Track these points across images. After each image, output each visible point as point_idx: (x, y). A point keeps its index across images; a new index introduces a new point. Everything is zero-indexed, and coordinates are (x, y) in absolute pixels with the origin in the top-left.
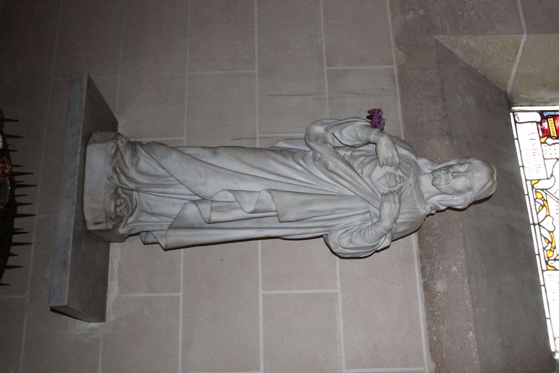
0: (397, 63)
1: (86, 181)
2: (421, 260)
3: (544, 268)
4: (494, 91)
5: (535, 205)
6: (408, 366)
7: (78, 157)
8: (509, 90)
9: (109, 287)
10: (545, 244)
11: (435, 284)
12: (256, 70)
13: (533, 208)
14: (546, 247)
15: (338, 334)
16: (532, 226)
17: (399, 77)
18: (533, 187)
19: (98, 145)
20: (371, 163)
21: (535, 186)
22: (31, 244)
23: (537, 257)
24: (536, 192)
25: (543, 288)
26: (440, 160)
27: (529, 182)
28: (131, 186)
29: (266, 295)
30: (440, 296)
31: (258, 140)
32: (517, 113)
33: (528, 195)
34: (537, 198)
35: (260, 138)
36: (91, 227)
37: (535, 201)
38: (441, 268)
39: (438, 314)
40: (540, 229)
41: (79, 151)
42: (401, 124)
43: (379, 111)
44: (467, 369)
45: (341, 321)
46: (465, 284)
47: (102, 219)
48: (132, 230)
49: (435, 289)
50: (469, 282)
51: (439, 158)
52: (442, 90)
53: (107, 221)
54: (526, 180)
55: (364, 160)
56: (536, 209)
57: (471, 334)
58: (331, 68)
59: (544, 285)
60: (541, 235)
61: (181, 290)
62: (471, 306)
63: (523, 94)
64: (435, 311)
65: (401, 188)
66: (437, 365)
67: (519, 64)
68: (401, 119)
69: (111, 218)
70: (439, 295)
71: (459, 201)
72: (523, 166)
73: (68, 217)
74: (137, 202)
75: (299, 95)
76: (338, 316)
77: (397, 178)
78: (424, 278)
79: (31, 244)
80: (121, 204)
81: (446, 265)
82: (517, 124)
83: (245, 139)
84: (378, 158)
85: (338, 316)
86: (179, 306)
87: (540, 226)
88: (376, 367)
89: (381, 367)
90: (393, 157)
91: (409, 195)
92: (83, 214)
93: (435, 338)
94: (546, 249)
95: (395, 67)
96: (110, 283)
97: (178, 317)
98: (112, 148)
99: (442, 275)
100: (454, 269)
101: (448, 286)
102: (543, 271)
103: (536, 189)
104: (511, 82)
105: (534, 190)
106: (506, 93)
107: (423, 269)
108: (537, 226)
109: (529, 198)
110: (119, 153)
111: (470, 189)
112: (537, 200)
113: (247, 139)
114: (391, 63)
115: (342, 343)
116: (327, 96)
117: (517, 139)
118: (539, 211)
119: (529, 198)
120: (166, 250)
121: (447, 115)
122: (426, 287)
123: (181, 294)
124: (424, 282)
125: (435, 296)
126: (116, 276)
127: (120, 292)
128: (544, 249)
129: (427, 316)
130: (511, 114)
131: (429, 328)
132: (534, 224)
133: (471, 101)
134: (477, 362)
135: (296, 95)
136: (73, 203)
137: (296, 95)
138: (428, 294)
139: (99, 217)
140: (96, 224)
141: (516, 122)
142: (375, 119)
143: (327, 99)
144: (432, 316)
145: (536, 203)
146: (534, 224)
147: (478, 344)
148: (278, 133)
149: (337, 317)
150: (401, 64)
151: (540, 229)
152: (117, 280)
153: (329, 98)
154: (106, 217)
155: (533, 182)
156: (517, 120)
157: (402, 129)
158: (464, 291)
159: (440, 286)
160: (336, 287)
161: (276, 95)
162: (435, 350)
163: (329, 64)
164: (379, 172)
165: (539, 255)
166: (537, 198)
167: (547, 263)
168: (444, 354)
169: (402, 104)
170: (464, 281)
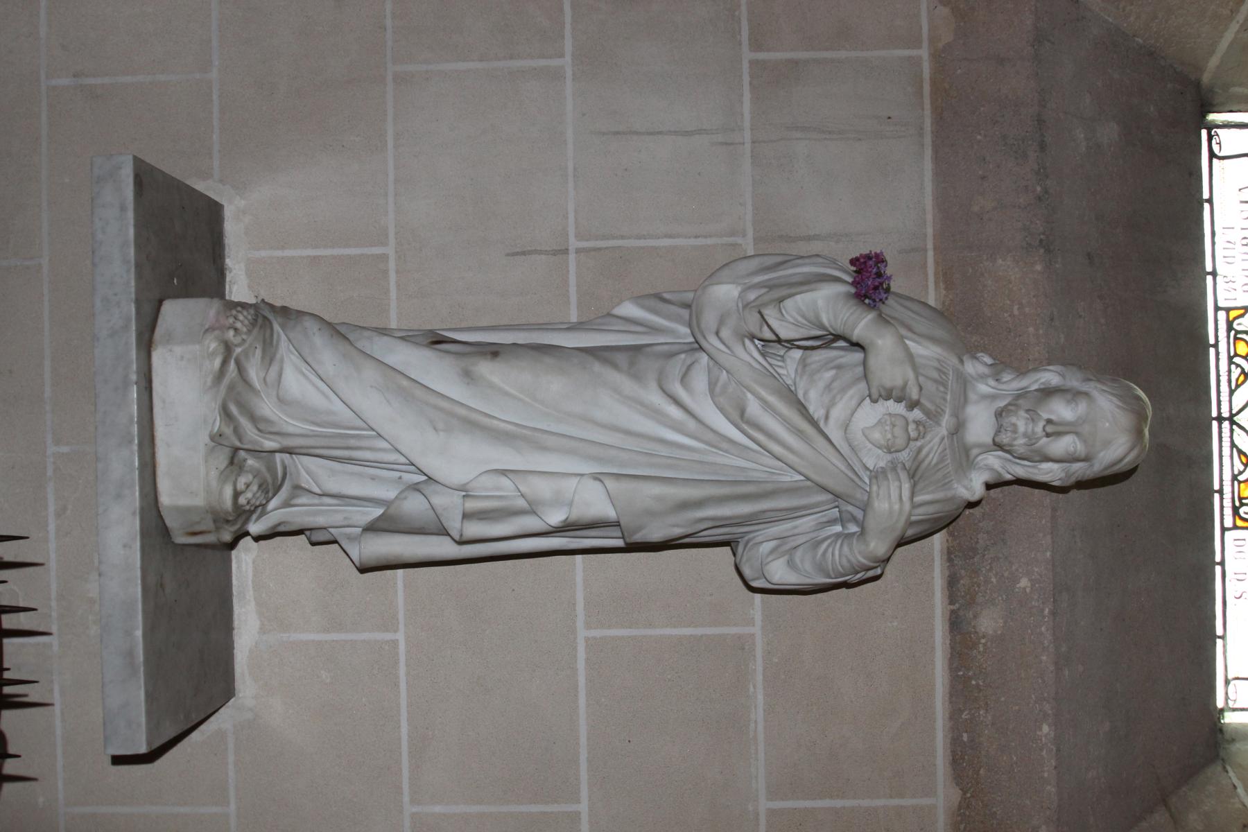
0: (933, 40)
1: (158, 442)
2: (950, 560)
3: (1228, 523)
4: (1169, 86)
5: (1229, 371)
6: (901, 796)
7: (134, 393)
8: (1206, 78)
9: (235, 616)
10: (1239, 466)
11: (975, 617)
12: (568, 58)
13: (1224, 379)
14: (1241, 473)
15: (753, 725)
16: (1215, 424)
17: (934, 82)
18: (1230, 327)
19: (178, 350)
20: (851, 392)
21: (1235, 326)
22: (52, 705)
23: (1217, 496)
24: (1236, 339)
25: (1218, 569)
26: (1016, 312)
27: (1222, 315)
28: (269, 444)
29: (595, 638)
30: (985, 645)
31: (572, 257)
32: (1219, 131)
33: (1216, 346)
34: (1236, 355)
35: (578, 251)
36: (181, 539)
37: (1230, 359)
38: (994, 580)
39: (978, 685)
40: (1232, 431)
41: (134, 377)
42: (929, 217)
43: (879, 259)
44: (1028, 802)
45: (760, 697)
46: (1044, 617)
47: (208, 524)
48: (279, 524)
49: (974, 627)
50: (1053, 614)
51: (1016, 307)
52: (1040, 121)
53: (218, 529)
54: (1217, 309)
55: (834, 379)
56: (1229, 381)
57: (1046, 729)
58: (762, 56)
59: (1222, 563)
60: (1233, 445)
61: (401, 626)
62: (1052, 668)
63: (1240, 85)
64: (970, 678)
65: (920, 450)
66: (965, 793)
67: (1242, 25)
68: (929, 202)
69: (228, 521)
70: (983, 641)
71: (1049, 472)
72: (1214, 274)
73: (125, 546)
74: (285, 468)
75: (676, 133)
76: (754, 687)
77: (912, 427)
78: (952, 602)
79: (52, 705)
80: (248, 485)
81: (1006, 574)
82: (1215, 161)
83: (540, 252)
84: (865, 376)
85: (754, 687)
86: (397, 662)
87: (1233, 423)
88: (831, 797)
89: (843, 798)
90: (905, 384)
91: (937, 464)
92: (161, 517)
93: (965, 737)
94: (1241, 478)
95: (924, 53)
96: (237, 609)
97: (397, 685)
98: (212, 355)
99: (995, 595)
100: (1024, 583)
101: (1005, 622)
102: (1224, 530)
103: (1237, 332)
104: (1214, 62)
105: (1233, 333)
106: (1198, 85)
107: (952, 582)
108: (1226, 424)
109: (1217, 354)
110: (232, 362)
111: (1086, 459)
112: (1236, 360)
113: (546, 252)
114: (915, 42)
115: (761, 747)
116: (747, 135)
117: (1210, 201)
118: (1238, 386)
119: (1217, 354)
120: (363, 570)
121: (1046, 192)
122: (955, 623)
123: (400, 637)
124: (952, 612)
125: (975, 645)
126: (251, 593)
127: (263, 630)
128: (1234, 478)
129: (952, 687)
130: (1204, 133)
131: (954, 715)
132: (1220, 419)
133: (1109, 132)
134: (1051, 789)
135: (670, 133)
136: (134, 513)
137: (670, 133)
138: (958, 638)
139: (198, 523)
140: (194, 534)
141: (1212, 155)
142: (869, 280)
143: (748, 146)
144: (965, 688)
145: (1233, 367)
146: (1220, 419)
147: (1058, 750)
148: (622, 237)
149: (752, 689)
150: (940, 45)
151: (1232, 431)
152: (253, 603)
153: (753, 142)
154: (215, 521)
155: (1233, 314)
156: (1216, 148)
157: (930, 231)
158: (1041, 634)
159: (988, 622)
160: (751, 622)
161: (617, 133)
162: (964, 760)
163: (756, 45)
164: (869, 415)
165: (1221, 492)
166: (1236, 355)
167: (1236, 511)
168: (982, 772)
169: (937, 158)
170: (1043, 610)
